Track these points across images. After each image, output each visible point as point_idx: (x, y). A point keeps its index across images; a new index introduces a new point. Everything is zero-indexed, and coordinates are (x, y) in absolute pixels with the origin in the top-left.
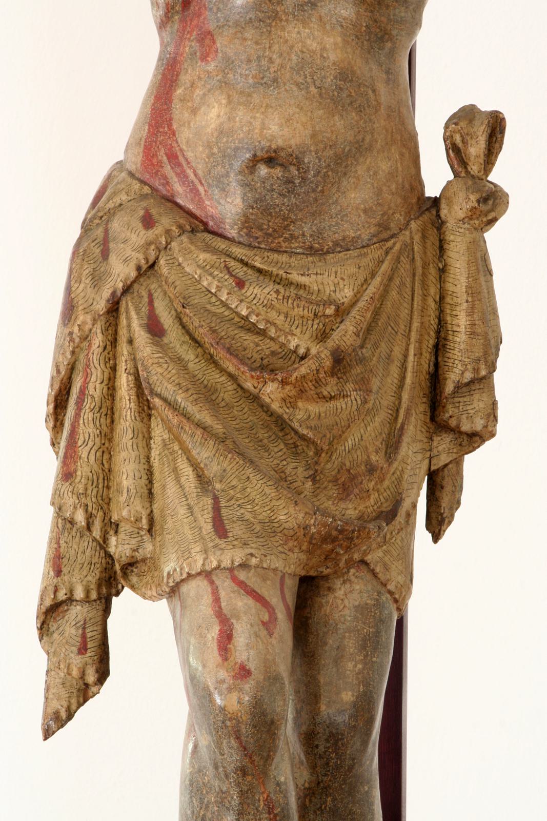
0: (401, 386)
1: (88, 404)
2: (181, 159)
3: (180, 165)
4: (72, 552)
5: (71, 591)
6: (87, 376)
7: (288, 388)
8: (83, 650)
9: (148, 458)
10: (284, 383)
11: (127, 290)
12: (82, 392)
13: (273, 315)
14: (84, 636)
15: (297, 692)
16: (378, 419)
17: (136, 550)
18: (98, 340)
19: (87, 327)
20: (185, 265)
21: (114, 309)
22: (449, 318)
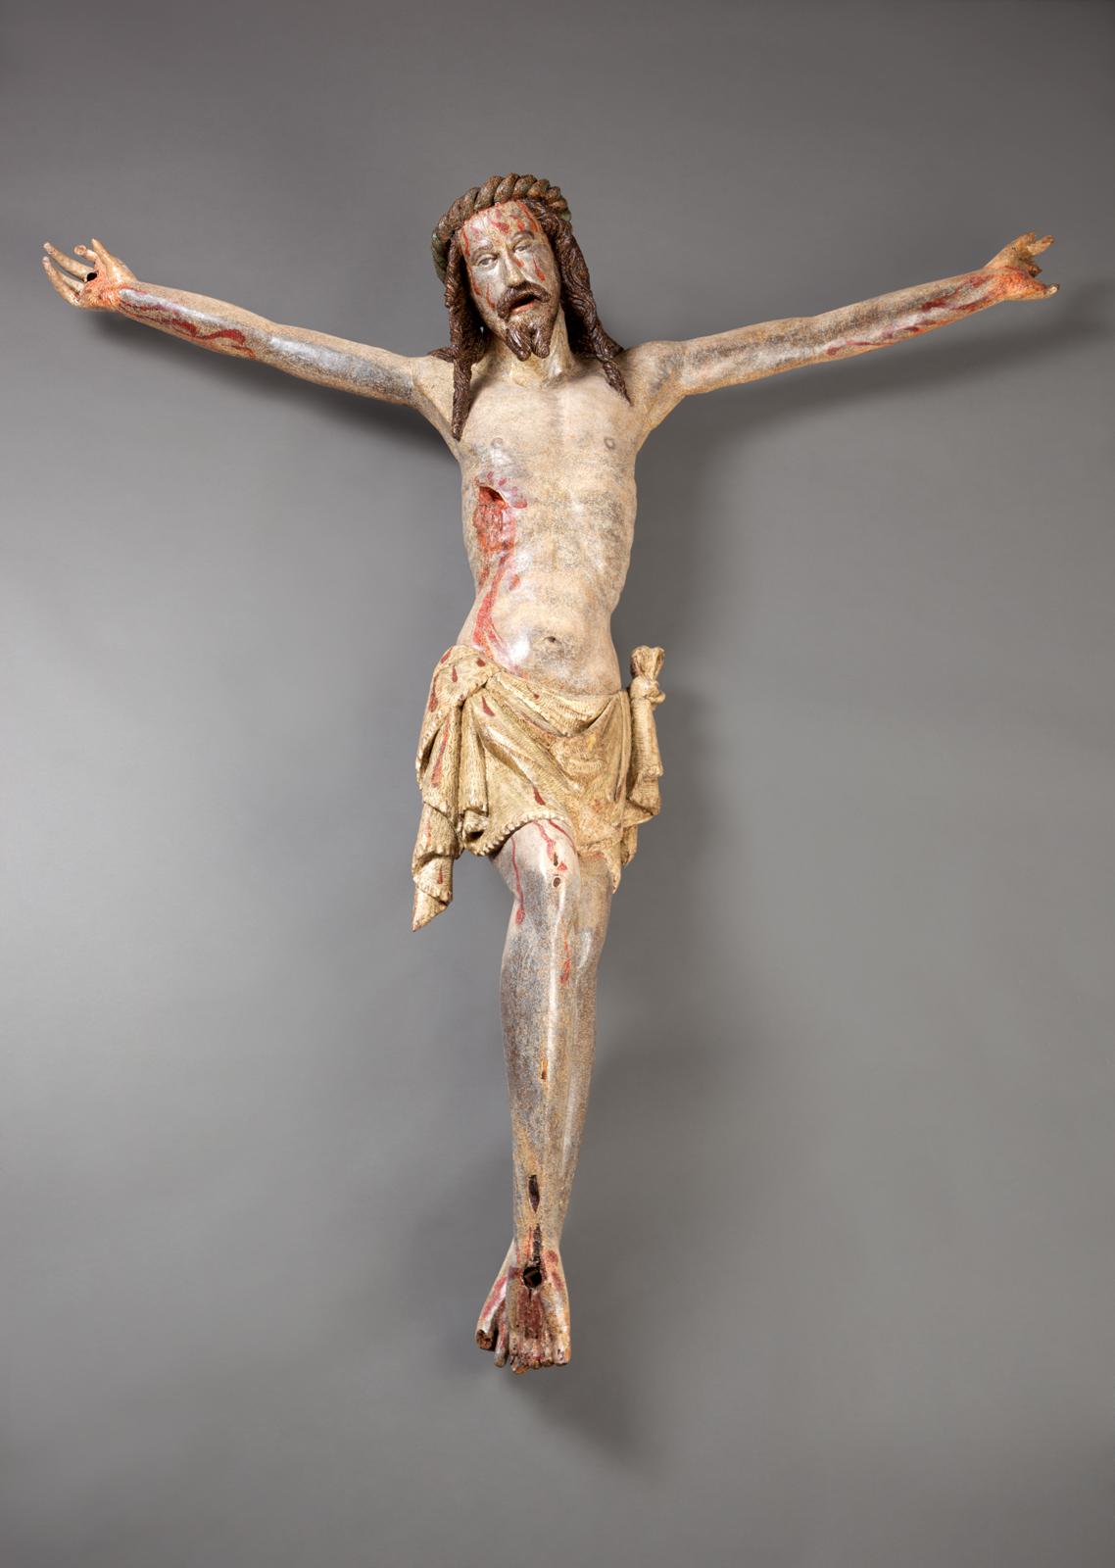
0: (619, 768)
1: (447, 750)
2: (497, 638)
3: (496, 641)
4: (436, 827)
5: (436, 847)
6: (446, 736)
7: (567, 747)
8: (440, 881)
9: (485, 777)
10: (555, 486)
11: (471, 695)
12: (444, 744)
13: (554, 715)
14: (441, 874)
15: (708, 383)
16: (550, 1045)
17: (477, 825)
18: (453, 719)
19: (447, 712)
20: (504, 684)
21: (461, 707)
22: (638, 745)
